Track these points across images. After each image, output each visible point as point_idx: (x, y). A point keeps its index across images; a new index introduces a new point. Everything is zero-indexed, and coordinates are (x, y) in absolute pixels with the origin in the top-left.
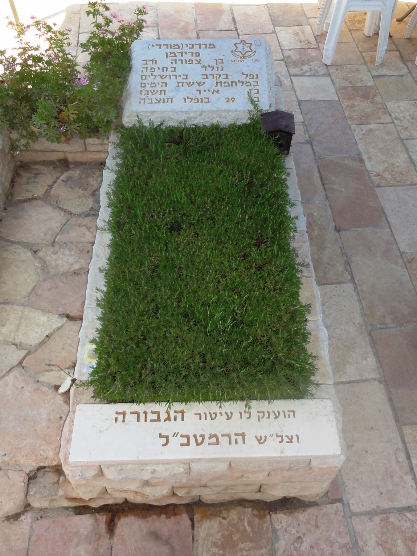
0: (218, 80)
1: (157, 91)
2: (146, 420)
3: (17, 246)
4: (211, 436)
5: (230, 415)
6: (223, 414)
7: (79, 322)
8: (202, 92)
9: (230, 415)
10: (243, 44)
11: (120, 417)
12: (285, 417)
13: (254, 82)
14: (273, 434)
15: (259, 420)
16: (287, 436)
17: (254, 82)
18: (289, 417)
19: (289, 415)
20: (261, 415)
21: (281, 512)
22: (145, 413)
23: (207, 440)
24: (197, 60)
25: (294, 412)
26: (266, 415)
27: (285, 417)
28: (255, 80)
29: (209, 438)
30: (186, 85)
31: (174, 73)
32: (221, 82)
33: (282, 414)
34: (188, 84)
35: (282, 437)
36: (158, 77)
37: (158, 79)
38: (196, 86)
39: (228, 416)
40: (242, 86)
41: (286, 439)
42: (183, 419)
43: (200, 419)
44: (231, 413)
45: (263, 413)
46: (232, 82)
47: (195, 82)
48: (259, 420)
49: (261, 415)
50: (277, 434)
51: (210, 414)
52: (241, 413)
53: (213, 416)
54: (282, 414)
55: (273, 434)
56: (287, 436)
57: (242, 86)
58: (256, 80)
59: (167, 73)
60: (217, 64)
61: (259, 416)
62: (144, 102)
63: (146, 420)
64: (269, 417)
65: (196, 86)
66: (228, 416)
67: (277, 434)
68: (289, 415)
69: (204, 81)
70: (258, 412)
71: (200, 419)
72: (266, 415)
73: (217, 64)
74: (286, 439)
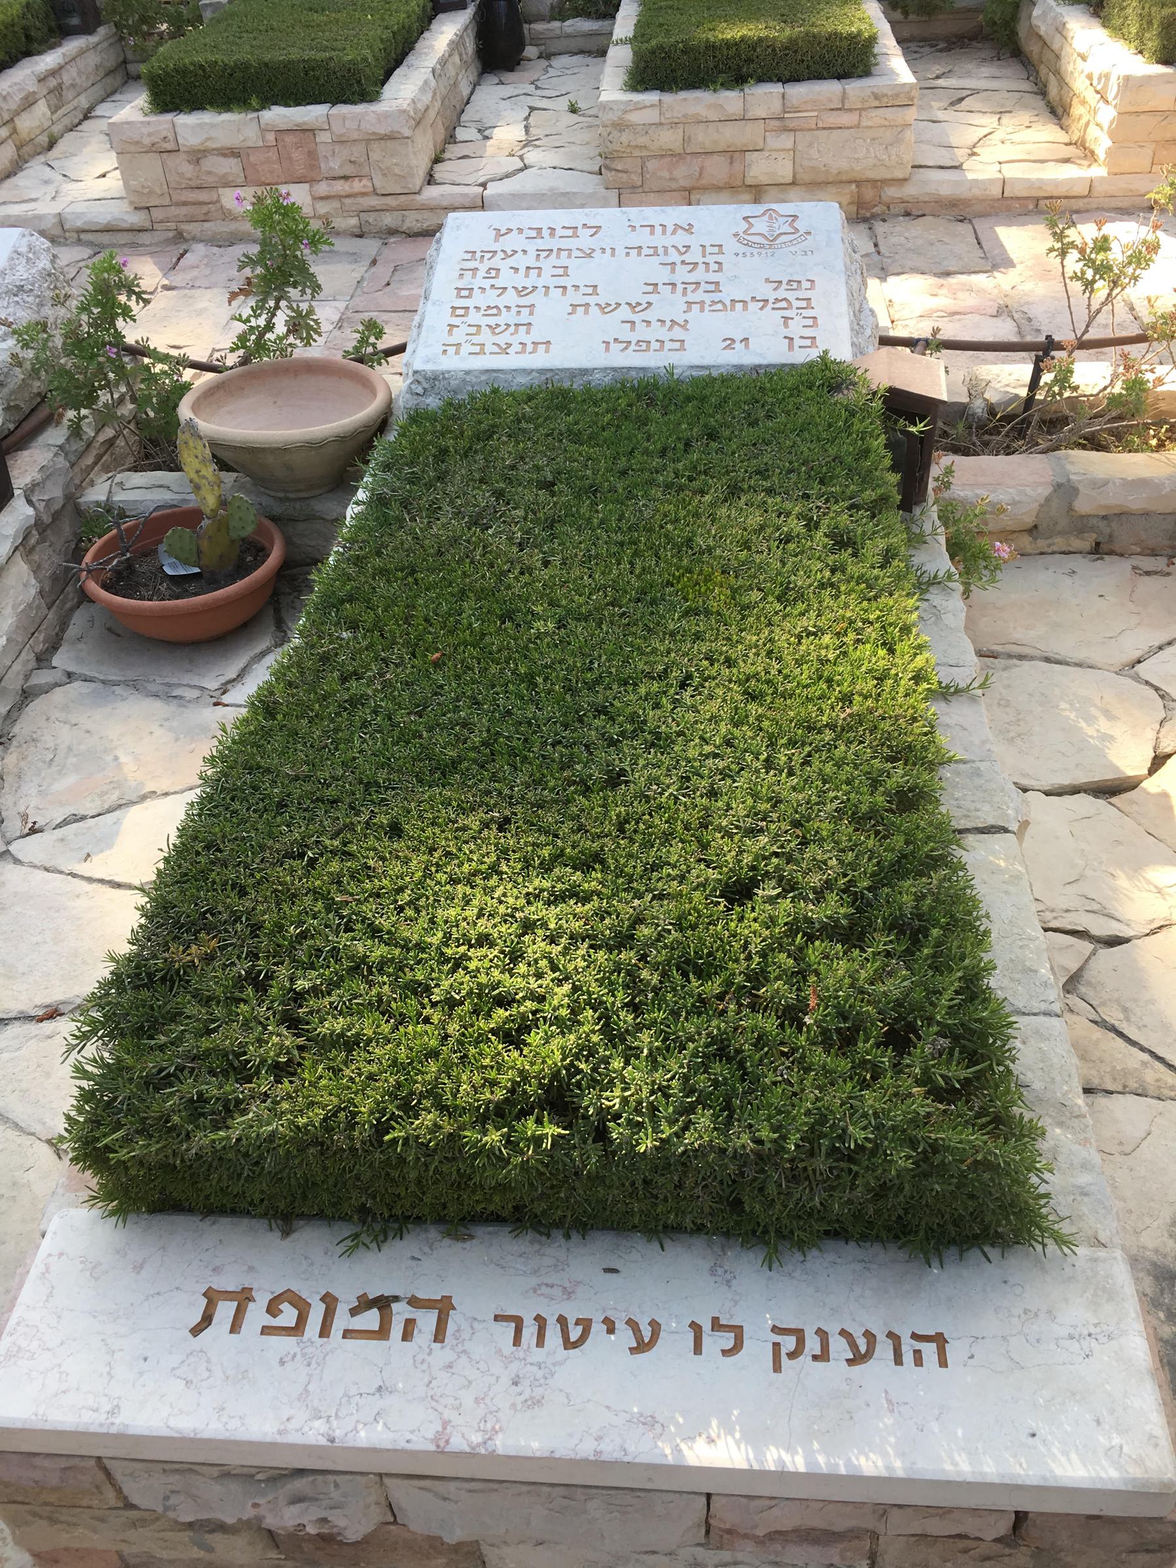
0: (691, 297)
1: (508, 325)
2: (325, 1332)
5: (647, 1334)
6: (620, 1325)
8: (640, 326)
9: (647, 1334)
10: (771, 217)
12: (898, 1360)
13: (797, 299)
15: (777, 1368)
17: (797, 299)
18: (407, 1336)
19: (918, 1354)
20: (789, 1343)
22: (330, 1302)
24: (498, 345)
25: (940, 1340)
26: (813, 1344)
27: (898, 1360)
28: (802, 294)
30: (594, 310)
31: (562, 281)
32: (702, 303)
33: (884, 1349)
34: (603, 308)
36: (511, 293)
37: (511, 298)
38: (624, 313)
39: (853, 1345)
40: (761, 309)
42: (943, 1363)
43: (517, 1341)
44: (655, 1326)
45: (799, 1334)
47: (623, 302)
48: (777, 1368)
49: (789, 1343)
51: (562, 1320)
52: (696, 1328)
53: (575, 1333)
54: (884, 1349)
57: (761, 309)
58: (808, 294)
59: (540, 283)
60: (704, 256)
61: (776, 1345)
62: (457, 353)
64: (823, 1356)
65: (624, 313)
66: (853, 1345)
68: (918, 1354)
69: (650, 298)
71: (517, 1341)
72: (813, 1344)
73: (704, 256)
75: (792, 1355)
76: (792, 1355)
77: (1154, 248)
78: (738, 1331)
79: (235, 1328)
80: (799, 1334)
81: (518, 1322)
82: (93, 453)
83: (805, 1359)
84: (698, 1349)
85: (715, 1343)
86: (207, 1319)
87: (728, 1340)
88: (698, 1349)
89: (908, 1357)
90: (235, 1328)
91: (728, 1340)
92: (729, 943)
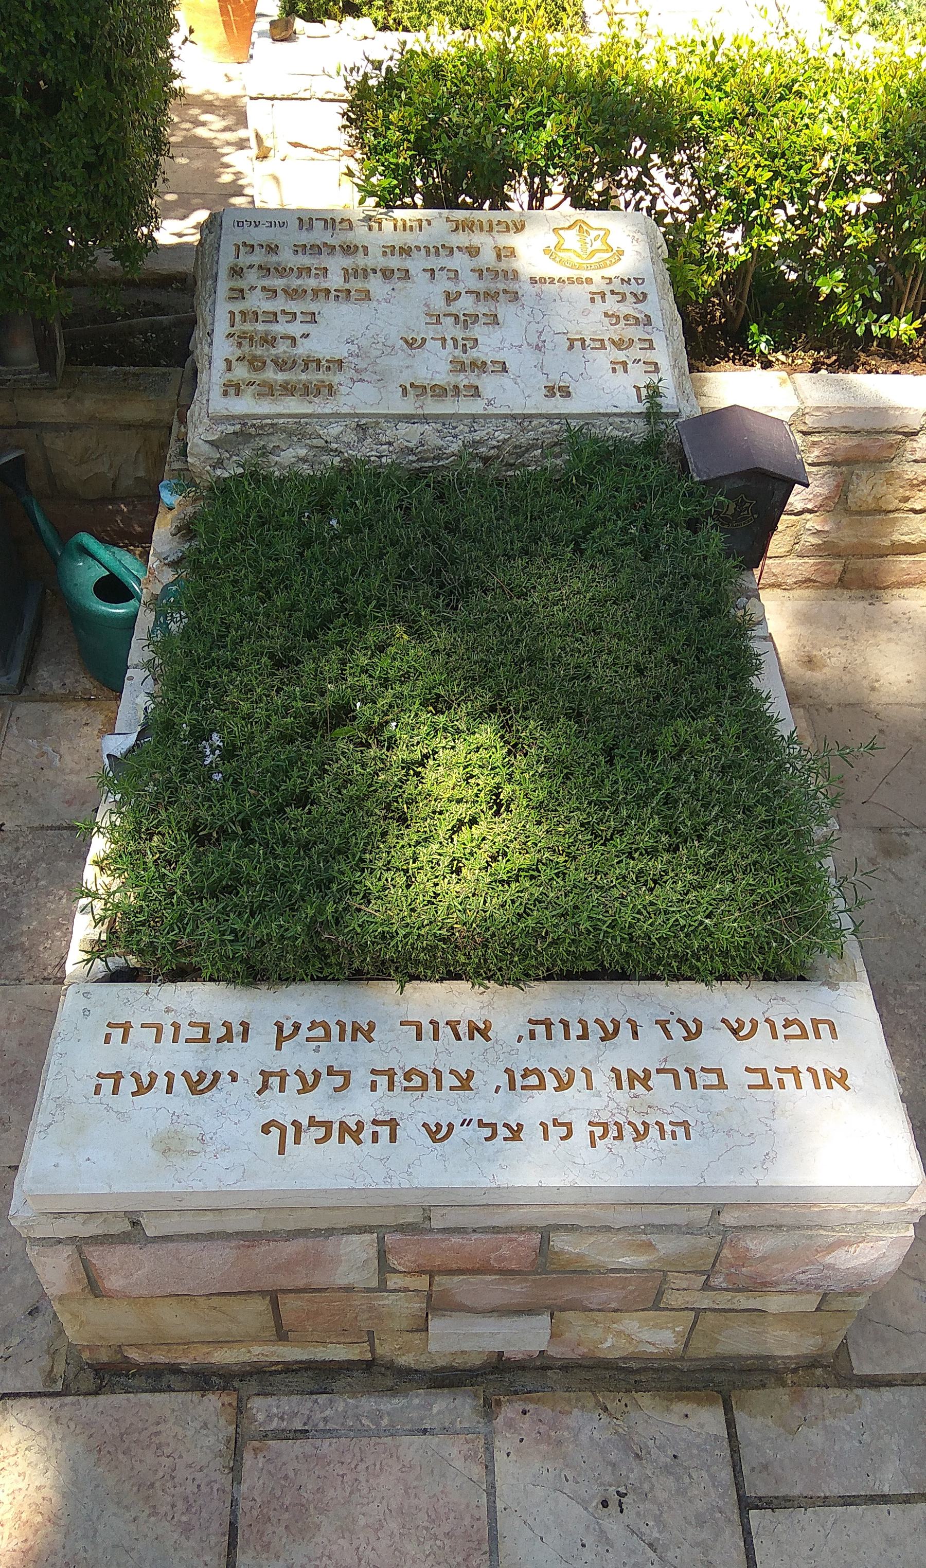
3: (905, 592)
4: (313, 1025)
7: (271, 1333)
11: (118, 1033)
14: (471, 1120)
16: (506, 1125)
20: (599, 1131)
21: (876, 700)
23: (304, 1032)
29: (310, 1029)
35: (493, 1126)
39: (604, 1028)
41: (503, 1132)
46: (815, 1023)
48: (593, 1144)
49: (599, 1131)
50: (480, 1121)
55: (471, 1120)
56: (506, 1125)
61: (592, 1133)
63: (175, 1040)
64: (620, 1137)
66: (604, 1028)
67: (480, 1121)
68: (673, 1133)
70: (590, 1124)
74: (503, 1132)
75: (602, 1137)
76: (602, 1137)
77: (458, 247)
78: (569, 1125)
79: (282, 1089)
80: (605, 1125)
81: (444, 340)
82: (296, 283)
83: (608, 1140)
84: (546, 1138)
85: (556, 1132)
86: (265, 1086)
87: (563, 1131)
88: (546, 1138)
89: (668, 1136)
90: (282, 1089)
91: (563, 1131)
92: (653, 1473)
